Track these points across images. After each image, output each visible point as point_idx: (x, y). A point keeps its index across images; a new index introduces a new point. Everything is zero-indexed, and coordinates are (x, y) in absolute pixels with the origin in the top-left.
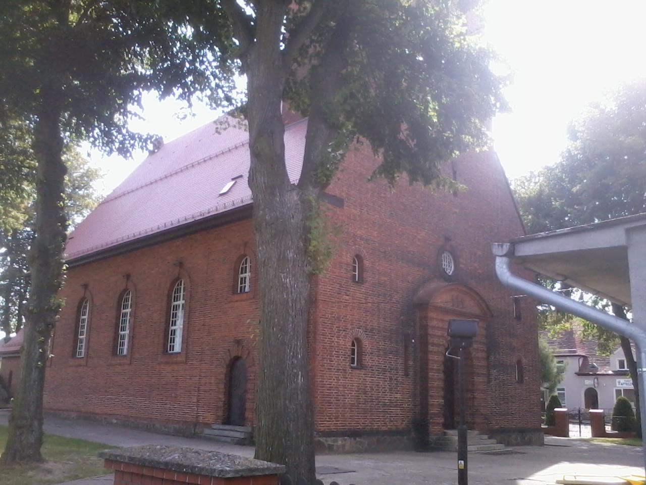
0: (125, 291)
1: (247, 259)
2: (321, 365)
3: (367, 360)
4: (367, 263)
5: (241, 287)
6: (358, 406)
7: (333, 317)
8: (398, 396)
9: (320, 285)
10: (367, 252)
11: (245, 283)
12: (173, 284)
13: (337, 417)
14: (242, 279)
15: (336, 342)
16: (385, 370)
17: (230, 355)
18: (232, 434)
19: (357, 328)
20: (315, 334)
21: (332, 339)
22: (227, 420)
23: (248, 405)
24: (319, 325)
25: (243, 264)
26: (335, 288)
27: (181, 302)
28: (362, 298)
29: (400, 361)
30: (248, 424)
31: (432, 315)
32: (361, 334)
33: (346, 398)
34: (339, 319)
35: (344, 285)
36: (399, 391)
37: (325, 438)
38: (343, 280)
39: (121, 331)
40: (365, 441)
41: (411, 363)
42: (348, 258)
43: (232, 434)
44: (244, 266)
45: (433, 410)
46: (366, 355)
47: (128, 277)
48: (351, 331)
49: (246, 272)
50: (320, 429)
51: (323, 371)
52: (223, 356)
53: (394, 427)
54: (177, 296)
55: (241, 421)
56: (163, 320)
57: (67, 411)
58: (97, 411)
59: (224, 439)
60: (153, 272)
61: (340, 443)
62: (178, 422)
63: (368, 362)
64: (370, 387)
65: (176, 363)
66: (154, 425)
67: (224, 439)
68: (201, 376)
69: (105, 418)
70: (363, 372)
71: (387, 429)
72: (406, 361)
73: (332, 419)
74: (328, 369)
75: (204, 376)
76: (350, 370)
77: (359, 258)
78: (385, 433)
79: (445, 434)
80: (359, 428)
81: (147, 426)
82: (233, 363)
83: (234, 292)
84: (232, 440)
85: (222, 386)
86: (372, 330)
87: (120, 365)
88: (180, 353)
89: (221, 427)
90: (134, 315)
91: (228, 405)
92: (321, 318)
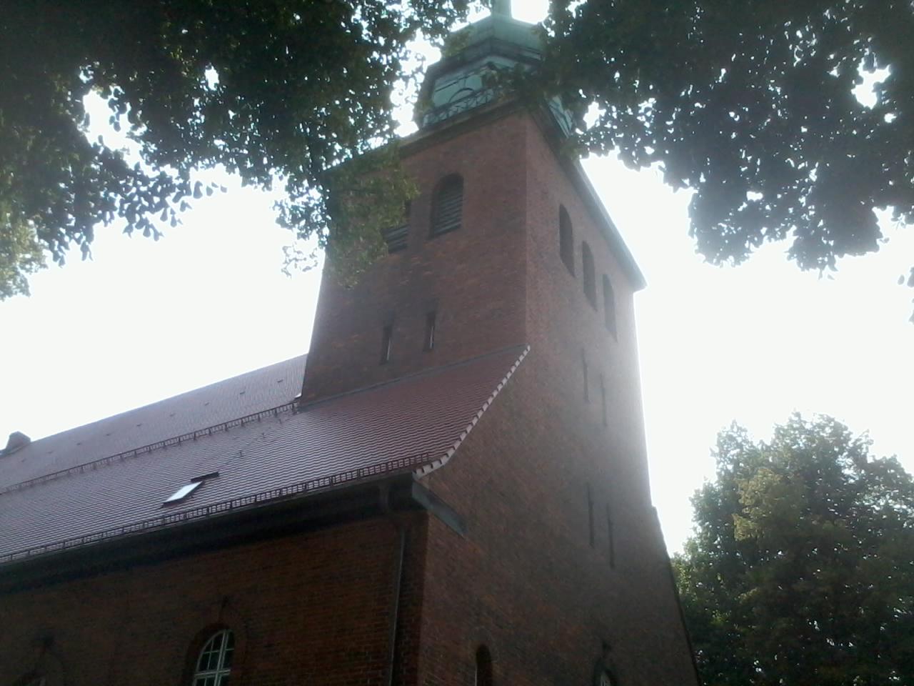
1: (221, 636)
4: (497, 670)
25: (208, 649)
42: (469, 652)
49: (213, 667)
77: (483, 656)
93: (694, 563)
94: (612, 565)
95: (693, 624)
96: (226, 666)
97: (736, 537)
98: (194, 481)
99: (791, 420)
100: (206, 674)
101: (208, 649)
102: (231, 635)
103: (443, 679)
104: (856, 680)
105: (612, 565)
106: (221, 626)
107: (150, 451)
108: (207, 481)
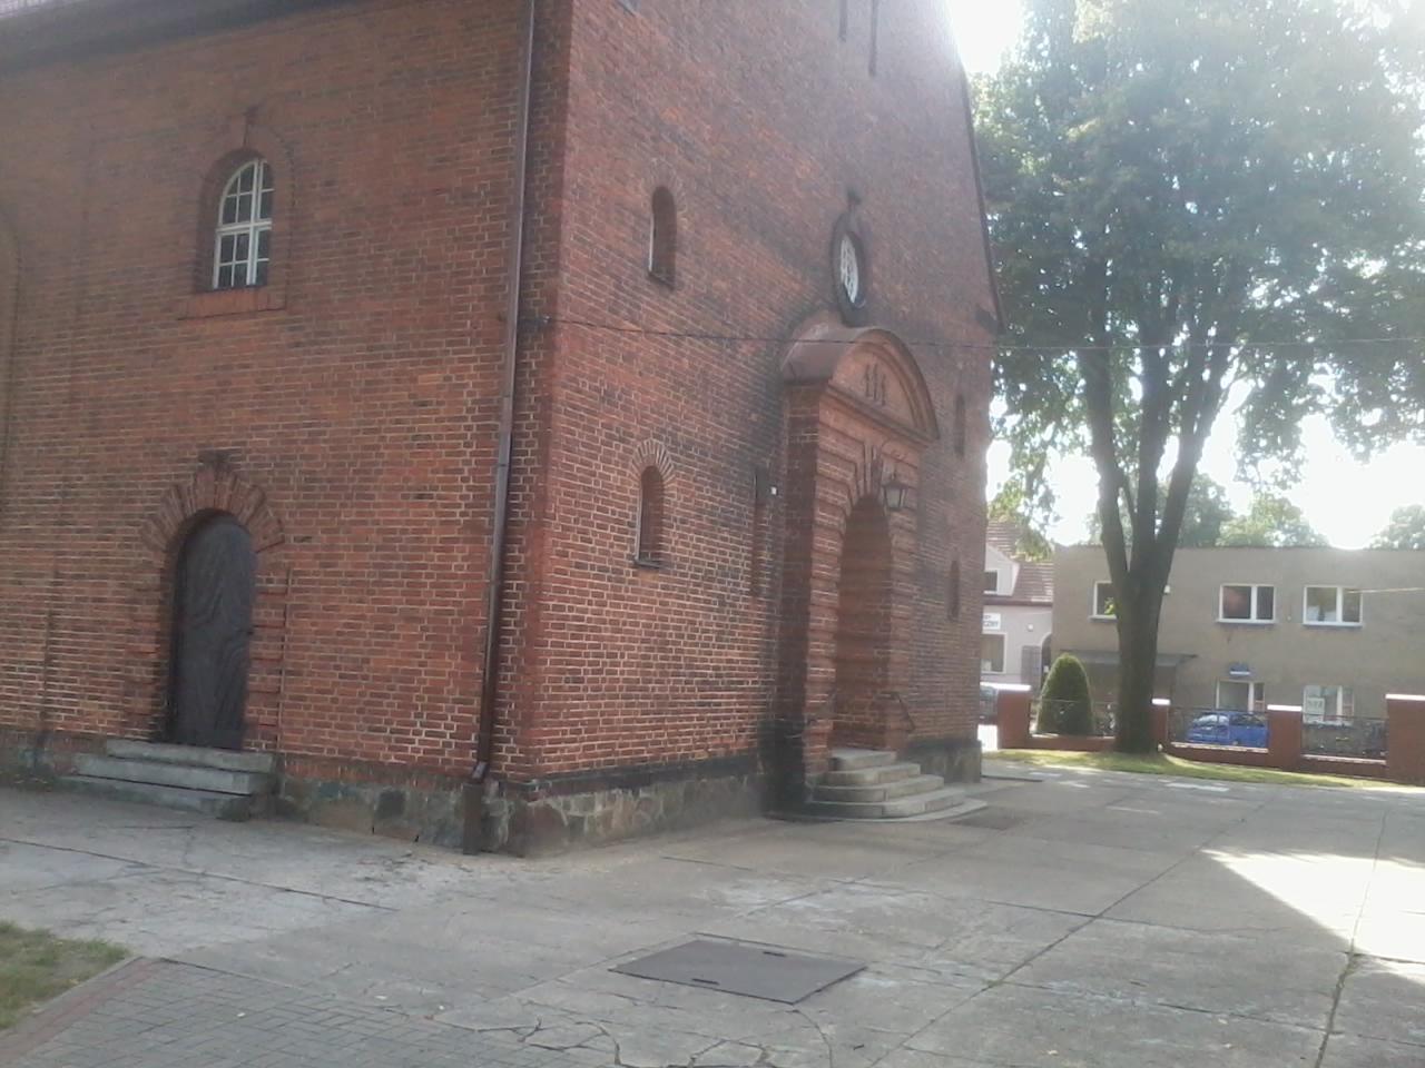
1: (253, 168)
3: (677, 543)
4: (684, 223)
5: (225, 272)
6: (646, 689)
8: (735, 654)
11: (243, 254)
14: (227, 242)
15: (601, 476)
18: (198, 777)
22: (169, 728)
23: (258, 679)
25: (233, 190)
26: (604, 288)
27: (254, 226)
30: (259, 745)
31: (829, 416)
32: (660, 454)
33: (617, 665)
37: (561, 799)
40: (655, 798)
41: (765, 556)
42: (640, 197)
43: (198, 777)
44: (239, 194)
45: (816, 698)
46: (672, 527)
48: (639, 445)
49: (245, 217)
50: (549, 768)
53: (721, 749)
55: (228, 731)
59: (168, 796)
63: (673, 550)
67: (168, 796)
68: (63, 576)
71: (705, 757)
73: (579, 731)
74: (578, 566)
76: (631, 570)
77: (663, 203)
79: (836, 764)
80: (644, 760)
84: (204, 801)
85: (147, 610)
89: (149, 751)
92: (565, 387)
93: (1002, 78)
94: (872, 71)
95: (988, 168)
96: (263, 216)
97: (1075, 37)
99: (1360, 17)
100: (235, 229)
102: (267, 168)
103: (602, 236)
104: (1216, 264)
105: (872, 71)
106: (246, 154)
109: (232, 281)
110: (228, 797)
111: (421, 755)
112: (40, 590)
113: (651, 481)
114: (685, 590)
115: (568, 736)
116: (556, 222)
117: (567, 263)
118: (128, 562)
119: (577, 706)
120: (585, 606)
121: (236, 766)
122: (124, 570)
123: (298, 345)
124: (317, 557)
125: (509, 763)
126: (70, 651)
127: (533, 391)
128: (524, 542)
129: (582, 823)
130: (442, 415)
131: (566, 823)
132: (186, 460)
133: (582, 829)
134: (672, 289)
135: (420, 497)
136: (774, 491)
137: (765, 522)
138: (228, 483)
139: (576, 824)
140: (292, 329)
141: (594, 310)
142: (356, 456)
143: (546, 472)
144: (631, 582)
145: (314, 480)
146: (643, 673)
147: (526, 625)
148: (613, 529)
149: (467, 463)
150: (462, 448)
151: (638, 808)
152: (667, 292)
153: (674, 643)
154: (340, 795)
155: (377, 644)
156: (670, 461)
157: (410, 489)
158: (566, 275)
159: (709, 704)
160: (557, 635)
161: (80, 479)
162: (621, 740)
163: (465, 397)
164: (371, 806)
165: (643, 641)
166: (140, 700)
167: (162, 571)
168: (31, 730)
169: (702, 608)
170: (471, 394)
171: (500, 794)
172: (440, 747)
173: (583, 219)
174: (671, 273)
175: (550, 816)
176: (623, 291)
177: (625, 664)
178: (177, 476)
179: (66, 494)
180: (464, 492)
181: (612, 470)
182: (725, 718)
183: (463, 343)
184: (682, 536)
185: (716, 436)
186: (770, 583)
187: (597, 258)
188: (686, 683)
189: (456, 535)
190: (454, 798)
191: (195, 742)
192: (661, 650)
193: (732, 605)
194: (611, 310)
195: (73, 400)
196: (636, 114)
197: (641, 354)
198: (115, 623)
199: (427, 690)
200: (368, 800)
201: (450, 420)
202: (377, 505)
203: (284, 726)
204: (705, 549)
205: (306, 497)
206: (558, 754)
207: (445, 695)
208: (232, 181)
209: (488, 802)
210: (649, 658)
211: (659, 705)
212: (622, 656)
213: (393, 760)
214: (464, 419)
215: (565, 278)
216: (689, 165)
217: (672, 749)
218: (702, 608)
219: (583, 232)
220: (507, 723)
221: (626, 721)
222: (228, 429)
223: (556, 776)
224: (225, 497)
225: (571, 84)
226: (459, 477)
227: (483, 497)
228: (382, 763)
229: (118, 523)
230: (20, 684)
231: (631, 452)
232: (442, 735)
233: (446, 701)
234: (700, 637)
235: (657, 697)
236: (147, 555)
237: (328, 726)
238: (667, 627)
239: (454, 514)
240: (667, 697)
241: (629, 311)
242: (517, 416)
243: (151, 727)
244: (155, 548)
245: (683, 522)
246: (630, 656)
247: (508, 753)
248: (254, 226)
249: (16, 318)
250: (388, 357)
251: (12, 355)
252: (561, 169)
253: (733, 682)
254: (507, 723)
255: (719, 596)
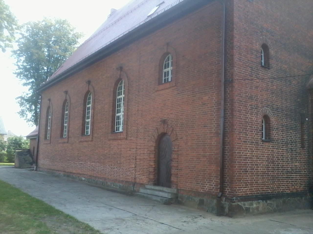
0: (88, 93)
1: (169, 56)
2: (238, 139)
3: (275, 134)
4: (272, 52)
5: (165, 80)
7: (247, 96)
8: (297, 164)
9: (236, 67)
10: (271, 43)
11: (168, 76)
12: (116, 84)
13: (252, 184)
14: (165, 73)
15: (250, 118)
16: (287, 143)
17: (158, 132)
18: (161, 194)
19: (266, 107)
20: (232, 110)
21: (246, 115)
22: (158, 182)
23: (173, 171)
24: (235, 102)
25: (166, 62)
26: (248, 70)
28: (269, 82)
29: (299, 135)
30: (174, 187)
33: (259, 167)
34: (251, 98)
35: (254, 69)
36: (297, 160)
37: (242, 203)
38: (254, 64)
39: (87, 119)
40: (274, 203)
41: (306, 137)
42: (258, 46)
43: (161, 194)
44: (167, 63)
47: (89, 82)
48: (261, 109)
49: (168, 67)
50: (239, 194)
51: (240, 144)
52: (153, 133)
54: (120, 92)
55: (168, 183)
56: (111, 109)
57: (59, 171)
58: (74, 172)
59: (154, 198)
60: (104, 77)
61: (255, 206)
62: (122, 181)
63: (274, 136)
64: (276, 157)
65: (120, 139)
66: (107, 183)
67: (154, 198)
69: (79, 177)
70: (271, 145)
72: (302, 135)
73: (248, 185)
74: (244, 142)
75: (139, 149)
76: (261, 142)
77: (265, 47)
78: (288, 195)
81: (103, 183)
82: (161, 138)
83: (160, 83)
84: (161, 199)
85: (152, 156)
86: (277, 109)
87: (86, 141)
88: (122, 132)
89: (153, 187)
90: (94, 108)
91: (158, 170)
92: (237, 96)
98: (157, 6)
101: (166, 62)
106: (168, 53)
107: (119, 20)
108: (161, 6)
109: (166, 81)
110: (166, 199)
111: (208, 190)
112: (134, 152)
113: (266, 118)
114: (279, 147)
115: (244, 186)
116: (232, 56)
117: (236, 65)
118: (149, 145)
119: (246, 178)
120: (247, 152)
121: (169, 191)
122: (148, 147)
123: (178, 94)
124: (184, 142)
125: (228, 193)
126: (139, 165)
127: (229, 98)
128: (228, 136)
129: (250, 209)
130: (209, 106)
131: (244, 209)
132: (158, 122)
133: (250, 211)
134: (269, 69)
135: (205, 126)
136: (307, 119)
137: (305, 128)
138: (166, 126)
139: (247, 210)
140: (177, 90)
141: (245, 76)
142: (191, 118)
143: (233, 118)
144: (261, 145)
145: (183, 124)
146: (267, 170)
147: (230, 157)
148: (255, 132)
149: (214, 117)
150: (213, 114)
151: (267, 205)
152: (267, 70)
153: (277, 161)
154: (190, 199)
155: (197, 163)
156: (272, 113)
157: (202, 125)
158: (235, 68)
159: (290, 178)
160: (239, 160)
161: (140, 128)
162: (261, 187)
163: (213, 101)
164: (197, 202)
165: (266, 161)
166: (152, 176)
167: (155, 147)
168: (132, 182)
169: (285, 152)
170: (215, 100)
171: (225, 201)
172: (212, 188)
173: (240, 54)
174: (269, 65)
175: (239, 207)
176: (254, 71)
177: (261, 167)
178: (157, 126)
179: (137, 131)
180: (214, 124)
181: (253, 117)
182: (295, 181)
183: (212, 88)
184: (277, 133)
185: (286, 106)
186: (308, 144)
187: (245, 63)
188: (281, 172)
189: (213, 135)
190: (215, 201)
191: (163, 185)
192: (272, 163)
193: (295, 151)
194: (250, 76)
195: (138, 111)
196: (255, 27)
197: (260, 86)
198: (147, 159)
199: (208, 174)
200: (196, 201)
201: (210, 107)
202: (196, 129)
203: (179, 182)
204: (285, 136)
205: (181, 128)
206: (241, 191)
207: (212, 175)
208: (166, 59)
209: (223, 203)
210: (269, 165)
211: (273, 178)
212: (260, 165)
213: (202, 191)
214: (214, 107)
215: (235, 69)
216: (272, 37)
217: (278, 190)
218: (285, 152)
219: (240, 57)
220: (227, 182)
221: (262, 182)
222: (166, 114)
223: (241, 197)
224: (166, 130)
225: (234, 22)
226: (213, 121)
227: (219, 125)
228: (199, 192)
229: (147, 137)
230: (131, 172)
231: (259, 111)
232: (212, 185)
233: (212, 177)
234: (285, 160)
235: (272, 176)
236: (152, 143)
237: (188, 182)
238: (274, 157)
239: (212, 130)
240: (275, 176)
241: (256, 75)
242: (225, 104)
243: (154, 182)
244: (153, 142)
245: (278, 129)
246: (262, 165)
247: (227, 190)
248: (170, 69)
249: (128, 95)
250: (196, 94)
251: (128, 103)
252: (233, 43)
253: (297, 172)
254: (227, 182)
255: (290, 148)
